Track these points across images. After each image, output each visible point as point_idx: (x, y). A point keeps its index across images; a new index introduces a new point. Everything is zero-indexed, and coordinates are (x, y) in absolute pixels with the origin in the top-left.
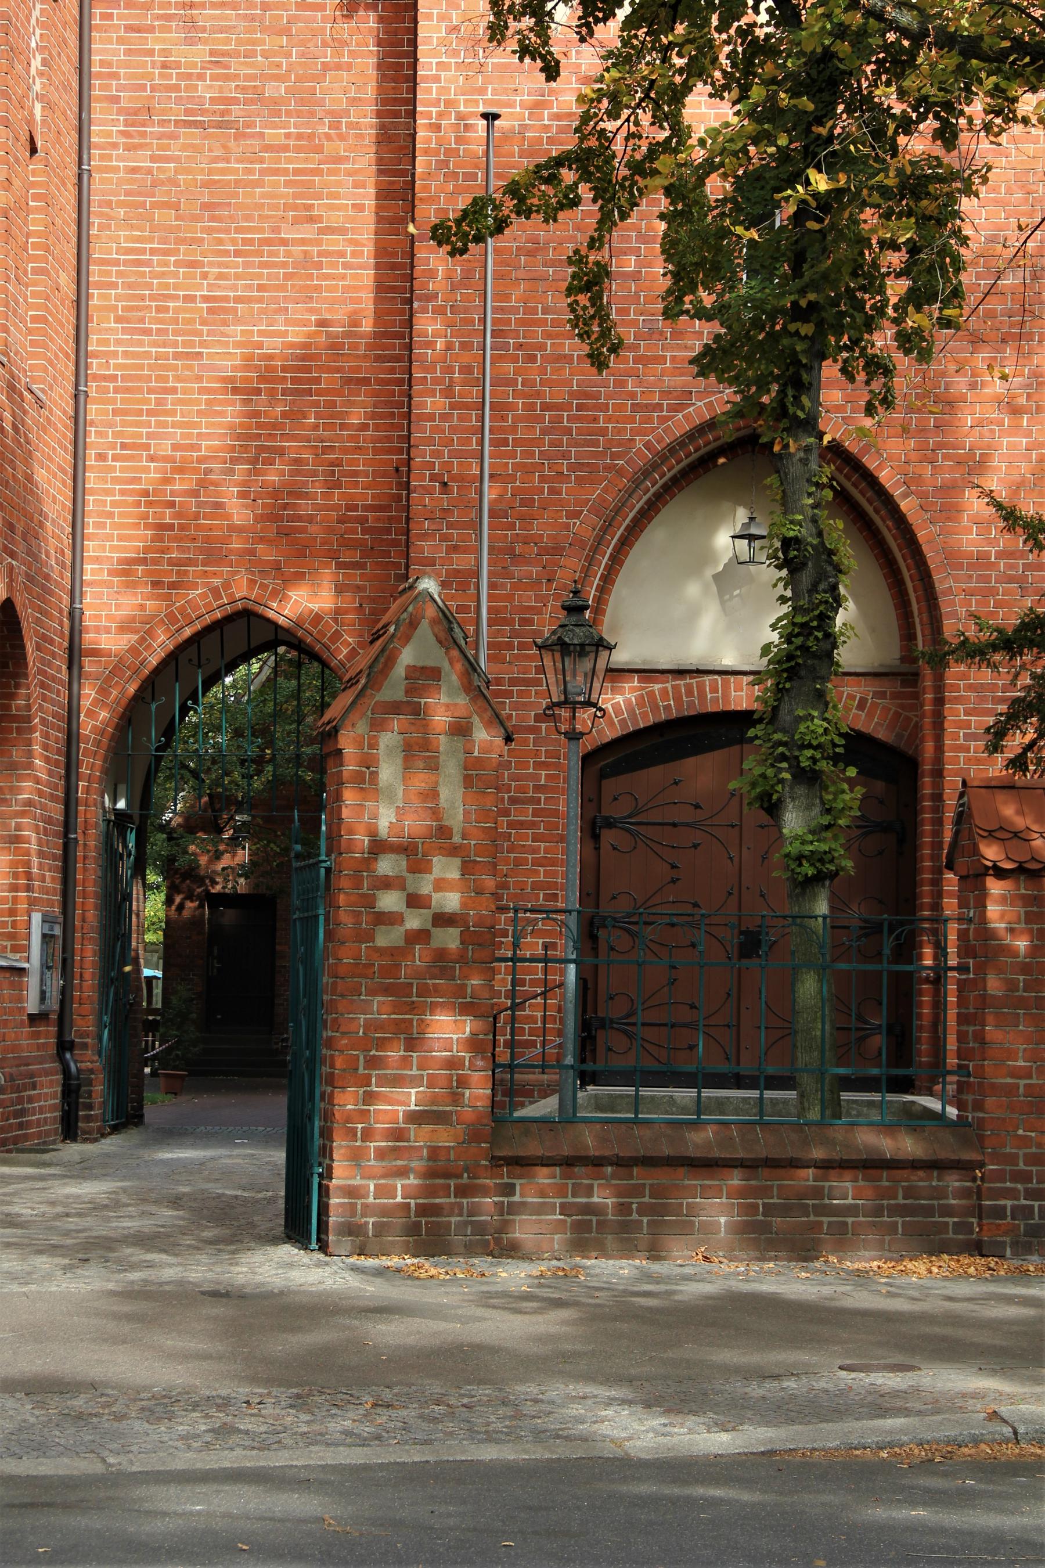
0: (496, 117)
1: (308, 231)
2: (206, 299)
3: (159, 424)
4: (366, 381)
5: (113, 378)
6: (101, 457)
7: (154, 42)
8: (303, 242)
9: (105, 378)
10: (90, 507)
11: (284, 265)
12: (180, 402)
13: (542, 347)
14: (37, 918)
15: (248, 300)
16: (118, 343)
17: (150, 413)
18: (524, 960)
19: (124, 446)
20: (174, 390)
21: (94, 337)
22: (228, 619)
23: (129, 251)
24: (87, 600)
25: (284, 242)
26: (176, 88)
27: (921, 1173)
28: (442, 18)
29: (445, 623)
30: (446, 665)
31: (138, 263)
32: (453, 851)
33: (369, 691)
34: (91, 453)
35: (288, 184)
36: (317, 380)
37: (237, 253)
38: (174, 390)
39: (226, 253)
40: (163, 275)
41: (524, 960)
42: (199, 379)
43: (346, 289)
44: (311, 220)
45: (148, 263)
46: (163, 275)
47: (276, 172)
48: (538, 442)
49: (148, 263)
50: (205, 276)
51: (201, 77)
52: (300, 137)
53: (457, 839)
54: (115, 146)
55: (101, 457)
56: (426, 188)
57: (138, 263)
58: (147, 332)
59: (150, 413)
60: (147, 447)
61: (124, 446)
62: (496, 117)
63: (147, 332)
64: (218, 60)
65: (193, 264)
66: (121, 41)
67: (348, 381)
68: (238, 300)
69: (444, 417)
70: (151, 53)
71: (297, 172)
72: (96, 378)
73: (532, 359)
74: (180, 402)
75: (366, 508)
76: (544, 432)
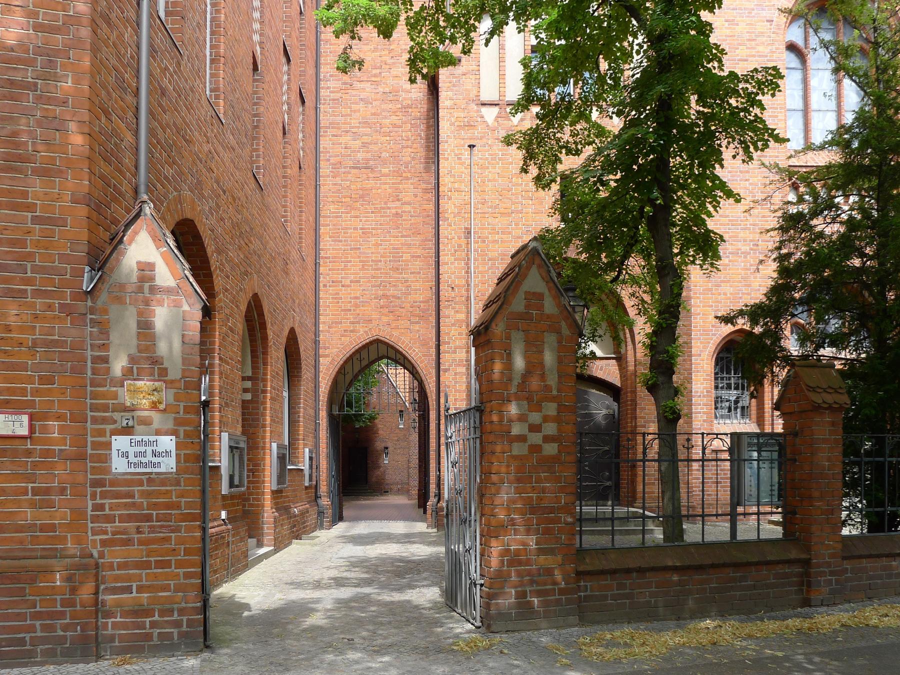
0: (474, 146)
1: (398, 204)
2: (361, 229)
3: (346, 274)
4: (419, 257)
5: (329, 258)
6: (325, 286)
7: (343, 140)
8: (396, 208)
9: (326, 258)
10: (321, 304)
11: (389, 216)
12: (353, 266)
13: (487, 238)
14: (307, 450)
15: (377, 229)
16: (330, 245)
17: (342, 270)
18: (648, 461)
19: (333, 282)
20: (350, 262)
21: (322, 244)
22: (371, 343)
23: (334, 213)
24: (321, 337)
25: (389, 208)
26: (350, 155)
27: (780, 566)
28: (448, 120)
29: (546, 267)
30: (547, 293)
31: (337, 217)
32: (553, 399)
33: (505, 306)
34: (321, 284)
35: (390, 188)
36: (402, 257)
37: (372, 212)
38: (350, 262)
39: (368, 212)
40: (346, 221)
41: (648, 461)
42: (359, 257)
43: (411, 224)
44: (398, 200)
45: (341, 217)
46: (346, 221)
47: (386, 184)
48: (487, 272)
49: (341, 217)
50: (361, 221)
51: (359, 152)
52: (394, 171)
53: (555, 392)
54: (328, 176)
55: (325, 286)
56: (444, 180)
57: (337, 217)
58: (341, 241)
59: (342, 270)
60: (341, 282)
61: (333, 282)
62: (474, 146)
63: (341, 241)
64: (365, 145)
65: (356, 217)
66: (330, 140)
67: (413, 257)
68: (373, 229)
69: (452, 263)
70: (341, 144)
71: (393, 184)
72: (323, 258)
73: (484, 242)
74: (353, 266)
75: (420, 302)
76: (489, 269)
